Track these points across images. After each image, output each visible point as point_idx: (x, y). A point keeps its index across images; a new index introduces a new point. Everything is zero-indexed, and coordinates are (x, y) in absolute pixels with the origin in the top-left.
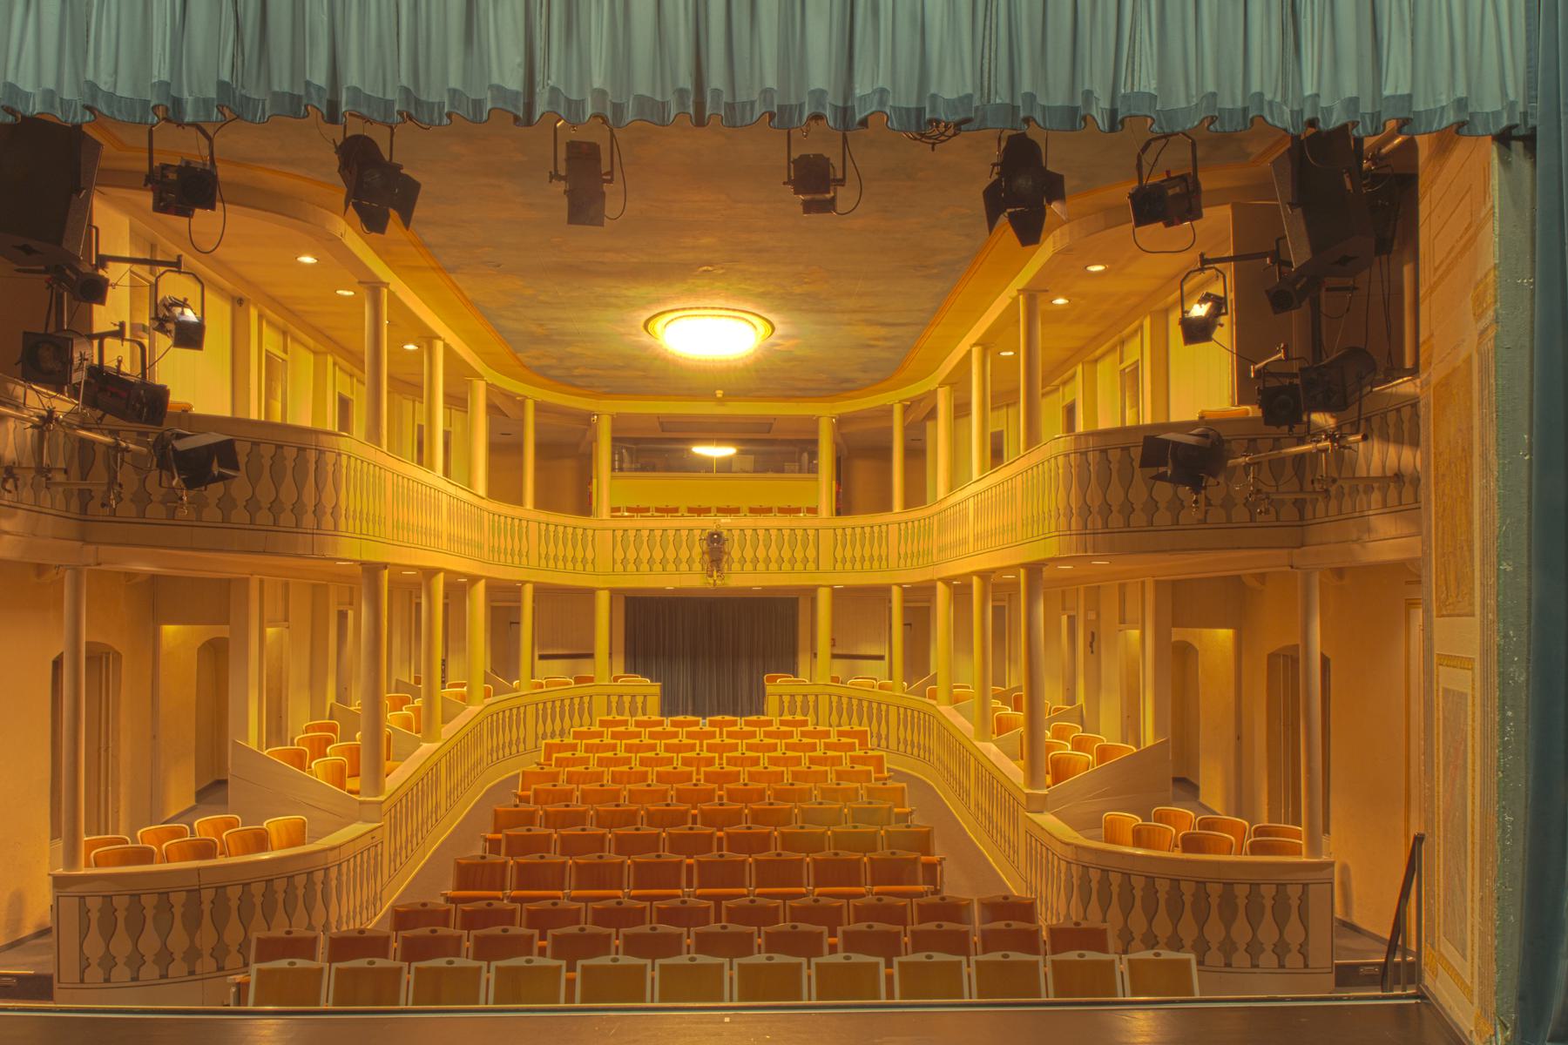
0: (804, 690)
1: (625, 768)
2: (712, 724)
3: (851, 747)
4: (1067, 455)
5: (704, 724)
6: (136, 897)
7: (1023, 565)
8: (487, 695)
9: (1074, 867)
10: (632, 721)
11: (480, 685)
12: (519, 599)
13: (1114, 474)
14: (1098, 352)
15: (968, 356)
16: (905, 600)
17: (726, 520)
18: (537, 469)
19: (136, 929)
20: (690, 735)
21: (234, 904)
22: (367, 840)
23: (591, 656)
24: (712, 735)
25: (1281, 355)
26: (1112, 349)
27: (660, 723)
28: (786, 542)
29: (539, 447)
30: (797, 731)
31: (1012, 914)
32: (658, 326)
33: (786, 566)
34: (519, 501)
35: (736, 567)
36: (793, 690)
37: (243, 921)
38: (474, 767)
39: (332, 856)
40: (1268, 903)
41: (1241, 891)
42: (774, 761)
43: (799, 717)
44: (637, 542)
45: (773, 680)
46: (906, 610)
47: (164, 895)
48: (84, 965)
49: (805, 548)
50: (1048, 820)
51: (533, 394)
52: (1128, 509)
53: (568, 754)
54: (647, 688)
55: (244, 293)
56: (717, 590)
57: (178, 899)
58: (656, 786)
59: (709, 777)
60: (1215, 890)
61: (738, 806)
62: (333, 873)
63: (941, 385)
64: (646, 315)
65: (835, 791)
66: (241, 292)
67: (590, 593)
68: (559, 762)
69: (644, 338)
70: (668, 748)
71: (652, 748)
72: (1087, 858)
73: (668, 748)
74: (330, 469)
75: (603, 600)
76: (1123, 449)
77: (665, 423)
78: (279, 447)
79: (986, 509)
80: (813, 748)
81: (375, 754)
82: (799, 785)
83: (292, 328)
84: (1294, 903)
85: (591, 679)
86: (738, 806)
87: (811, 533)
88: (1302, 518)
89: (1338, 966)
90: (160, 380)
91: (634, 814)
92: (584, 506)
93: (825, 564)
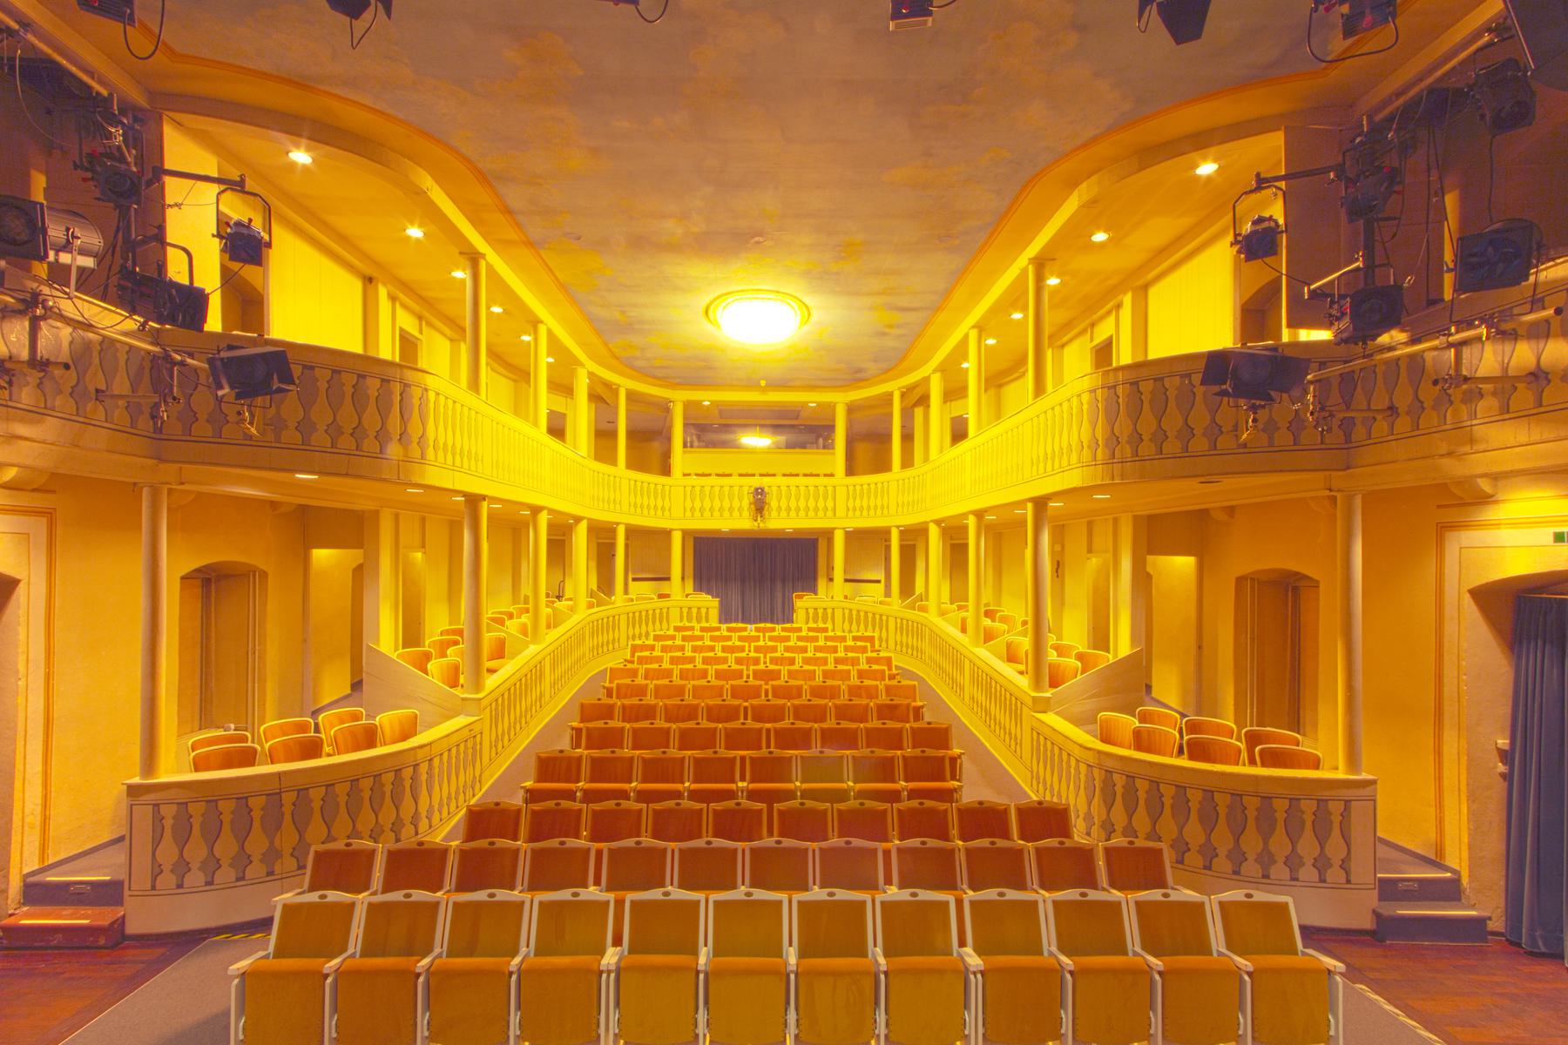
0: (824, 605)
1: (690, 666)
2: (758, 630)
3: (864, 650)
4: (1093, 391)
5: (751, 629)
6: (213, 803)
7: (1032, 500)
8: (591, 606)
9: (1096, 772)
10: (697, 626)
11: (583, 599)
12: (614, 538)
13: (1146, 405)
14: (1065, 339)
15: (966, 336)
16: (901, 540)
17: (766, 481)
18: (629, 447)
19: (212, 836)
20: (741, 639)
21: (317, 805)
22: (465, 733)
23: (668, 579)
24: (757, 639)
25: (1359, 264)
26: (1084, 331)
27: (718, 629)
28: (811, 496)
29: (631, 434)
30: (822, 636)
31: (1046, 820)
32: (718, 312)
33: (811, 514)
34: (614, 462)
35: (774, 514)
36: (816, 604)
37: (305, 828)
38: (578, 660)
39: (421, 754)
40: (1309, 818)
41: (1280, 806)
42: (807, 661)
43: (821, 625)
44: (705, 496)
45: (801, 597)
46: (902, 548)
47: (243, 800)
48: (157, 871)
49: (825, 499)
50: (1052, 719)
51: (625, 384)
52: (1160, 437)
53: (647, 653)
54: (709, 603)
55: (374, 274)
56: (761, 531)
57: (257, 803)
58: (714, 682)
59: (757, 675)
60: (1252, 804)
61: (782, 702)
62: (424, 768)
63: (935, 371)
64: (706, 299)
65: (859, 687)
66: (369, 272)
67: (666, 534)
68: (642, 660)
69: (708, 327)
70: (724, 649)
71: (712, 649)
72: (1110, 764)
73: (724, 649)
74: (416, 402)
75: (677, 540)
76: (1155, 380)
77: (723, 410)
78: (361, 377)
79: (1024, 444)
80: (835, 650)
81: (482, 653)
82: (830, 682)
83: (427, 315)
84: (1336, 819)
85: (668, 596)
86: (782, 702)
87: (830, 489)
88: (1348, 440)
89: (1381, 880)
90: (196, 284)
91: (696, 707)
92: (666, 470)
93: (841, 512)
